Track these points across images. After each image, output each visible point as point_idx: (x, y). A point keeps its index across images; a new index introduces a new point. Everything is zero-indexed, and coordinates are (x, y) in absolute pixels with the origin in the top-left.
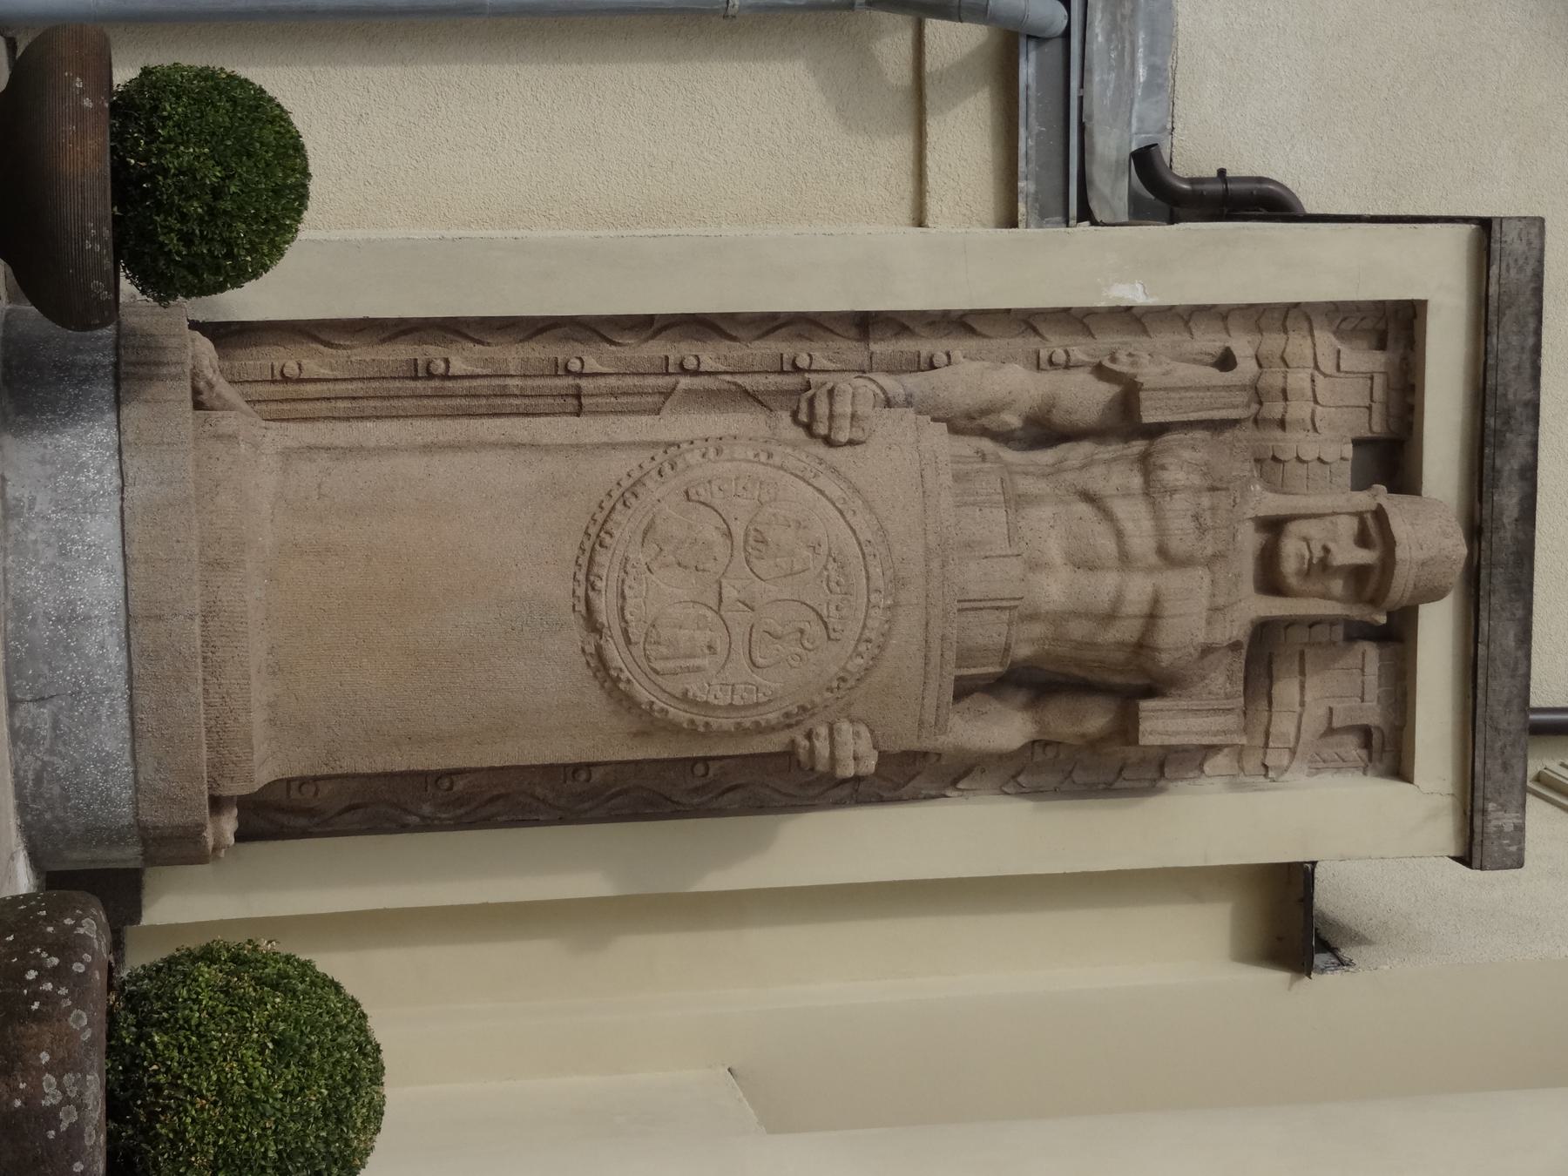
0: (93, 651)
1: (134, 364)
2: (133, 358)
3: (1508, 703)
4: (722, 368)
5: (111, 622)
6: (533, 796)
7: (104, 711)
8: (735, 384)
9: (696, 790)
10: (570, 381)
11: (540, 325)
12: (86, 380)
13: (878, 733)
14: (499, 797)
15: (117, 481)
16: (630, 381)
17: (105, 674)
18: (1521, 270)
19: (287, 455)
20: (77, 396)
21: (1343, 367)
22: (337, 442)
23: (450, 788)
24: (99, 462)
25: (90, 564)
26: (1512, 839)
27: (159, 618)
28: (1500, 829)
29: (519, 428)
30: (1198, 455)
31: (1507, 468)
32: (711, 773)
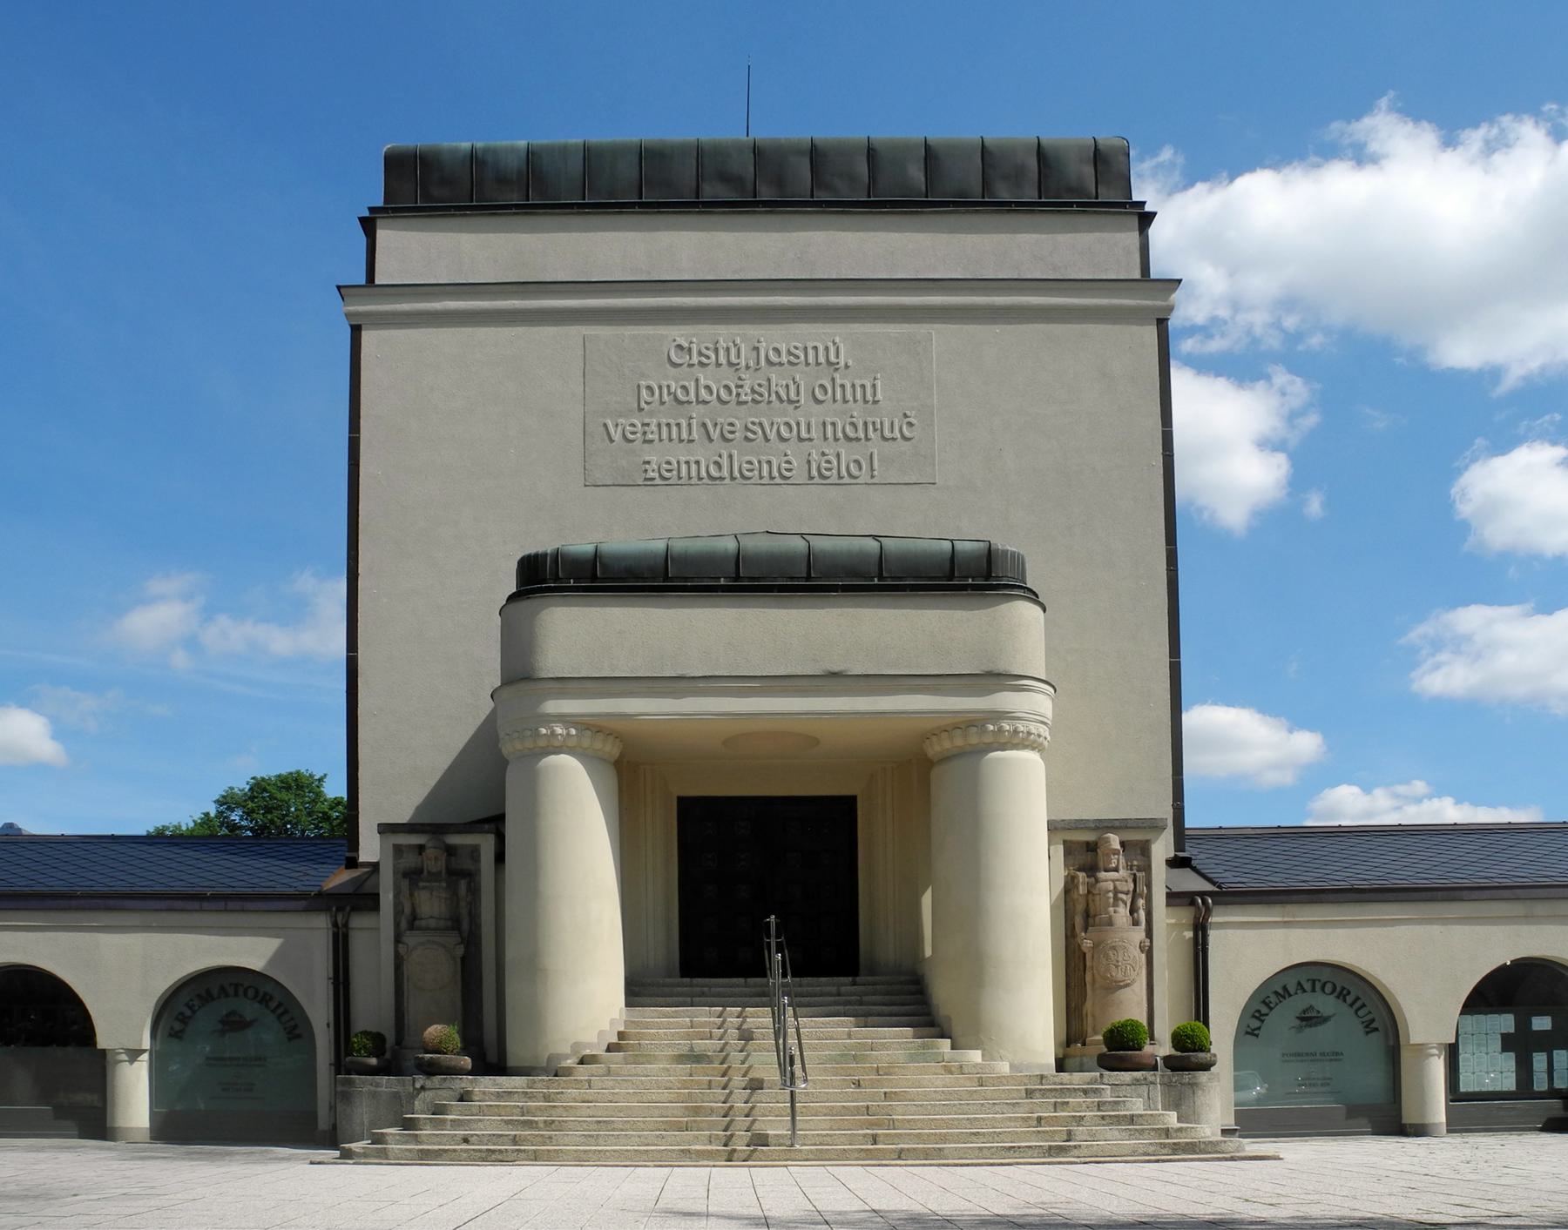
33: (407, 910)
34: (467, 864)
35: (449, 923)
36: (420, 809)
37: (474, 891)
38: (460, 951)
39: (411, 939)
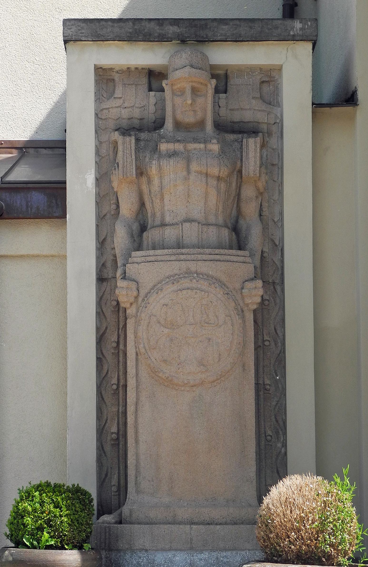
0: (203, 563)
1: (105, 544)
2: (104, 544)
3: (251, 28)
4: (117, 333)
5: (193, 556)
6: (276, 406)
7: (225, 560)
8: (122, 329)
9: (276, 344)
10: (121, 388)
11: (101, 399)
12: (110, 560)
13: (247, 278)
14: (276, 418)
15: (143, 552)
16: (121, 367)
17: (211, 559)
18: (82, 28)
19: (138, 492)
20: (115, 564)
21: (120, 96)
22: (134, 474)
23: (271, 436)
24: (137, 558)
25: (171, 562)
26: (305, 24)
27: (191, 539)
28: (301, 29)
29: (131, 409)
30: (148, 155)
31: (158, 31)
32: (269, 339)
33: (127, 208)
34: (247, 109)
35: (212, 234)
36: (40, 129)
37: (273, 166)
38: (255, 293)
39: (146, 269)
